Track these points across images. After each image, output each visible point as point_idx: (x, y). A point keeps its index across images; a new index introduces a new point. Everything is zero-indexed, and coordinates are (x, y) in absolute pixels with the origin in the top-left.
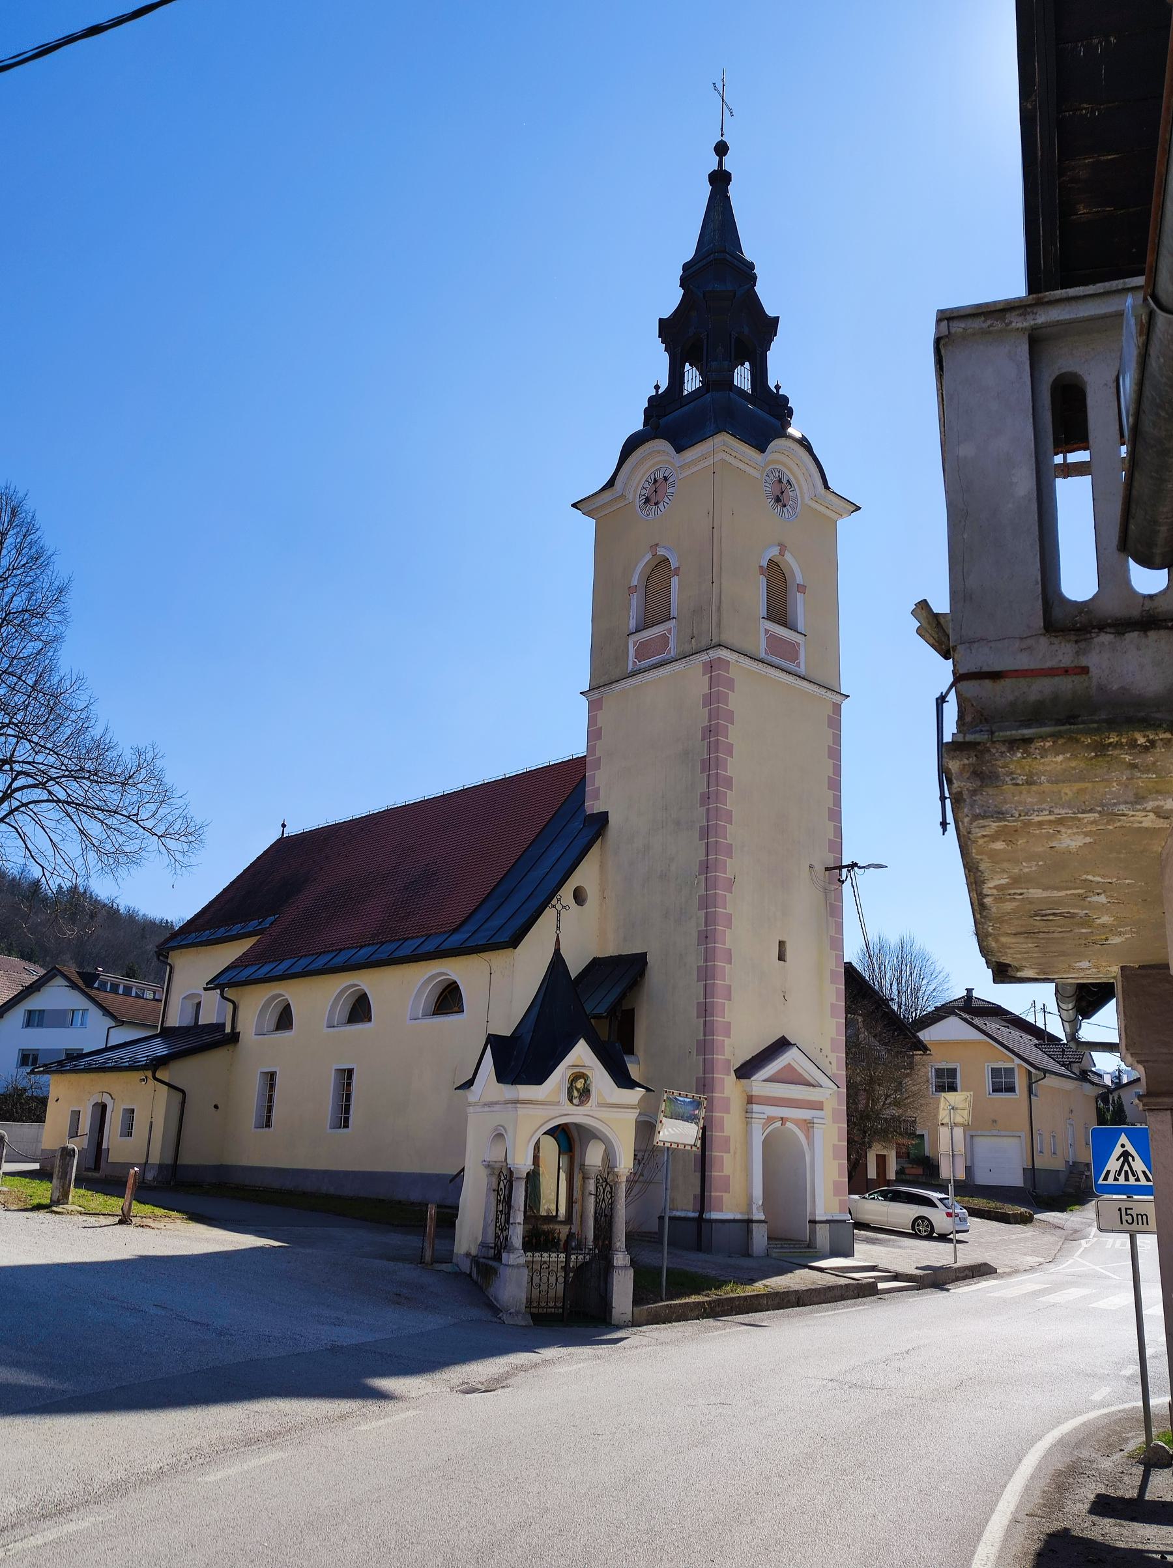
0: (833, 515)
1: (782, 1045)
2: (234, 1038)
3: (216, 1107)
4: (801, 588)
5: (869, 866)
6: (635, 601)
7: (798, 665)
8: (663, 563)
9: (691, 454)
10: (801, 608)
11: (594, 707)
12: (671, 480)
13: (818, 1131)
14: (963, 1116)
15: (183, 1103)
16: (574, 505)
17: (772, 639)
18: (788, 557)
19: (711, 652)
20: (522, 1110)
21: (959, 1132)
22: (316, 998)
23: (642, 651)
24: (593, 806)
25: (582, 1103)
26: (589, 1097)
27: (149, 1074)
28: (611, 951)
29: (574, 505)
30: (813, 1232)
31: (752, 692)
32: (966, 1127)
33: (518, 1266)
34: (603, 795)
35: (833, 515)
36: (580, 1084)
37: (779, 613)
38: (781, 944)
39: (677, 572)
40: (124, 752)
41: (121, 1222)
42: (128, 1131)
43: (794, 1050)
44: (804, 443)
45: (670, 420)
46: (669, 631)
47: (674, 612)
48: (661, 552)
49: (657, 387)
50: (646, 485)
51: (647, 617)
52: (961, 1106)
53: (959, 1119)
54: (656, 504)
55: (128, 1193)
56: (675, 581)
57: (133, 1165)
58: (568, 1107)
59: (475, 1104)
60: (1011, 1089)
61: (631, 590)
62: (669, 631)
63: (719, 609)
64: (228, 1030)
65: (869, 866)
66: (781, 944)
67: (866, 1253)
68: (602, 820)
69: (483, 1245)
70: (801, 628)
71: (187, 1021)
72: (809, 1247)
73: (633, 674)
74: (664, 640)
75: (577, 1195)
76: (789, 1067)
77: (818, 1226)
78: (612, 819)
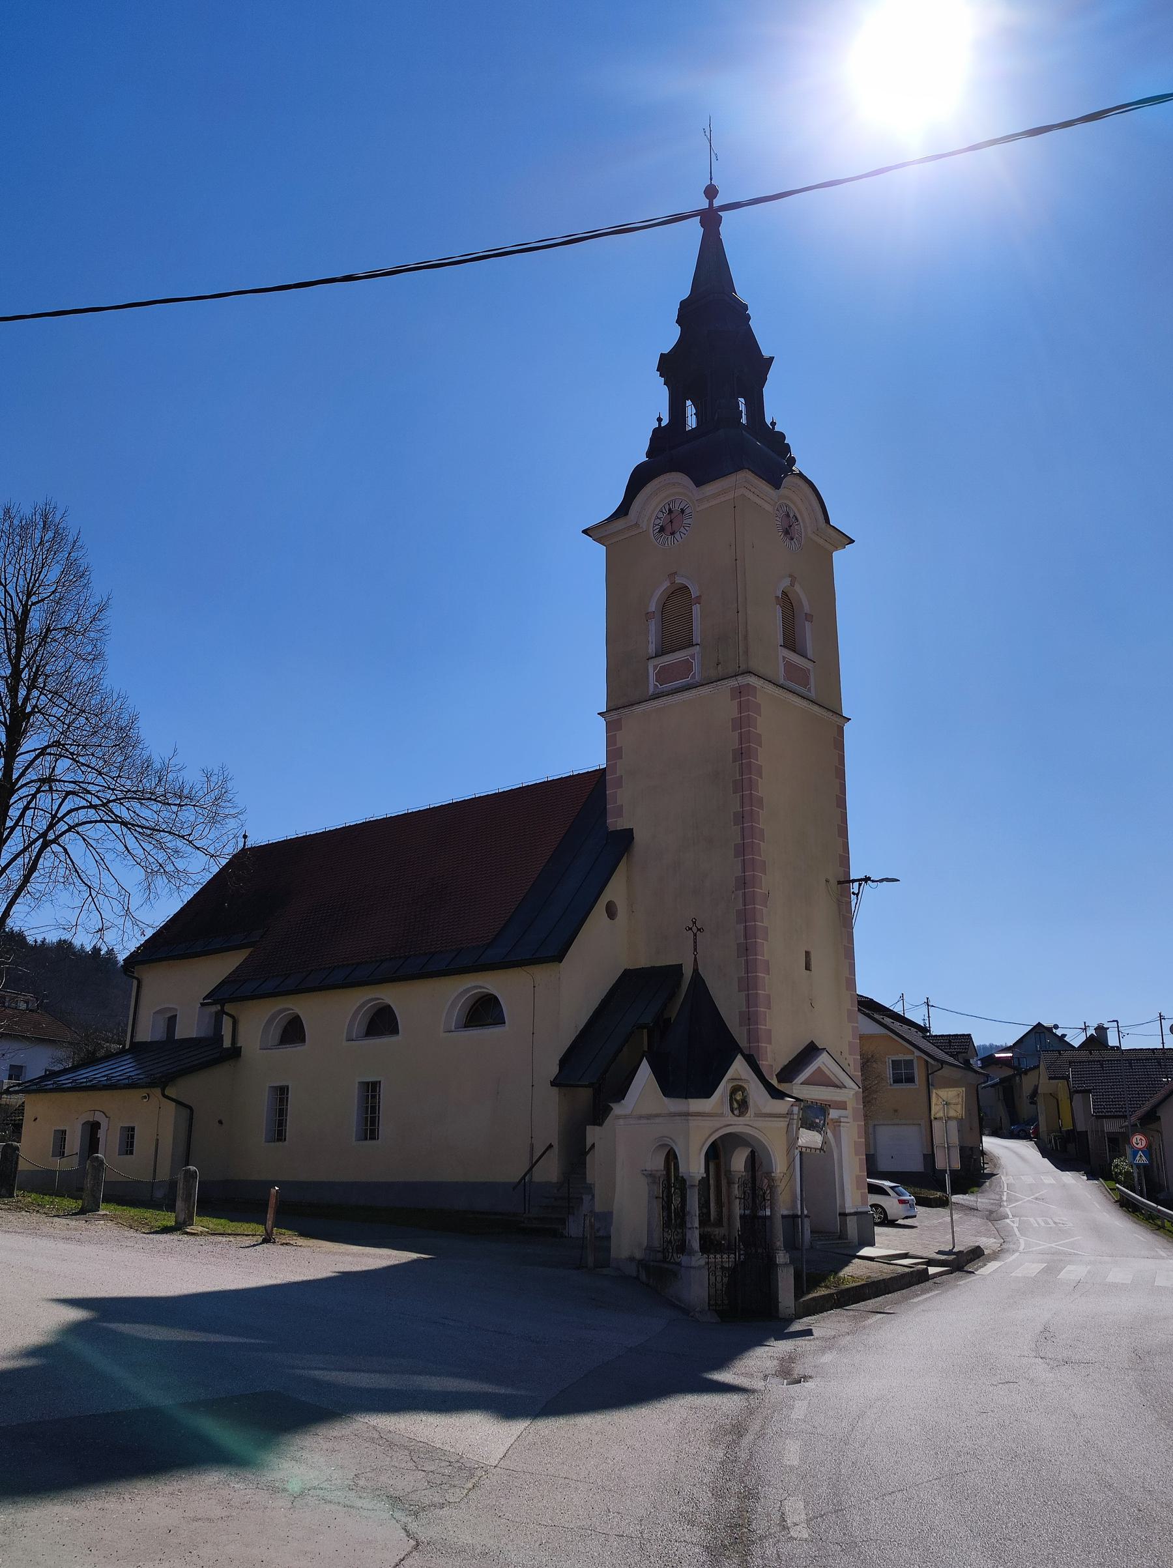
0: (827, 546)
1: (811, 1051)
2: (235, 1053)
3: (220, 1122)
4: (809, 618)
5: (881, 881)
6: (653, 626)
7: (809, 690)
8: (679, 593)
9: (710, 489)
10: (809, 634)
11: (613, 728)
12: (687, 511)
13: (844, 1130)
14: (957, 1111)
15: (191, 1118)
16: (585, 532)
17: (789, 666)
18: (797, 588)
19: (739, 678)
20: (694, 1123)
21: (953, 1125)
22: (331, 1015)
23: (664, 675)
24: (616, 823)
25: (741, 1114)
26: (747, 1108)
27: (158, 1091)
28: (643, 962)
29: (585, 532)
30: (844, 1224)
31: (777, 717)
32: (960, 1121)
33: (700, 1268)
34: (628, 809)
35: (827, 546)
36: (739, 1097)
37: (791, 642)
38: (807, 954)
39: (698, 600)
40: (191, 777)
41: (265, 1241)
42: (128, 1146)
43: (825, 1054)
44: (801, 475)
45: (668, 451)
46: (693, 656)
47: (697, 638)
48: (679, 580)
49: (660, 420)
50: (661, 515)
51: (666, 639)
52: (954, 1101)
53: (952, 1113)
54: (673, 533)
55: (270, 1215)
56: (696, 609)
57: (275, 1183)
58: (731, 1118)
59: (625, 1117)
60: (910, 1079)
61: (649, 616)
62: (693, 656)
63: (746, 637)
64: (227, 1043)
65: (881, 881)
66: (807, 954)
67: (886, 1242)
68: (626, 838)
69: (649, 1248)
70: (810, 654)
71: (160, 1035)
72: (840, 1238)
73: (657, 696)
74: (687, 665)
75: (724, 1199)
76: (819, 1069)
77: (848, 1218)
78: (638, 836)
